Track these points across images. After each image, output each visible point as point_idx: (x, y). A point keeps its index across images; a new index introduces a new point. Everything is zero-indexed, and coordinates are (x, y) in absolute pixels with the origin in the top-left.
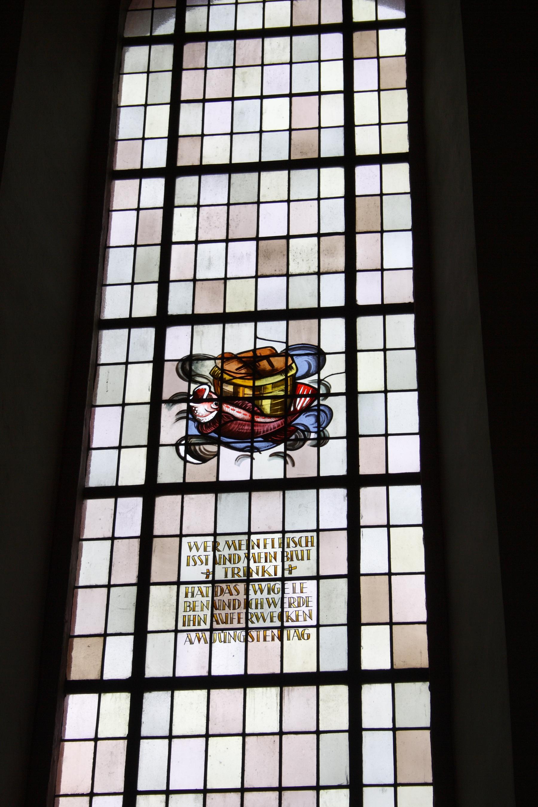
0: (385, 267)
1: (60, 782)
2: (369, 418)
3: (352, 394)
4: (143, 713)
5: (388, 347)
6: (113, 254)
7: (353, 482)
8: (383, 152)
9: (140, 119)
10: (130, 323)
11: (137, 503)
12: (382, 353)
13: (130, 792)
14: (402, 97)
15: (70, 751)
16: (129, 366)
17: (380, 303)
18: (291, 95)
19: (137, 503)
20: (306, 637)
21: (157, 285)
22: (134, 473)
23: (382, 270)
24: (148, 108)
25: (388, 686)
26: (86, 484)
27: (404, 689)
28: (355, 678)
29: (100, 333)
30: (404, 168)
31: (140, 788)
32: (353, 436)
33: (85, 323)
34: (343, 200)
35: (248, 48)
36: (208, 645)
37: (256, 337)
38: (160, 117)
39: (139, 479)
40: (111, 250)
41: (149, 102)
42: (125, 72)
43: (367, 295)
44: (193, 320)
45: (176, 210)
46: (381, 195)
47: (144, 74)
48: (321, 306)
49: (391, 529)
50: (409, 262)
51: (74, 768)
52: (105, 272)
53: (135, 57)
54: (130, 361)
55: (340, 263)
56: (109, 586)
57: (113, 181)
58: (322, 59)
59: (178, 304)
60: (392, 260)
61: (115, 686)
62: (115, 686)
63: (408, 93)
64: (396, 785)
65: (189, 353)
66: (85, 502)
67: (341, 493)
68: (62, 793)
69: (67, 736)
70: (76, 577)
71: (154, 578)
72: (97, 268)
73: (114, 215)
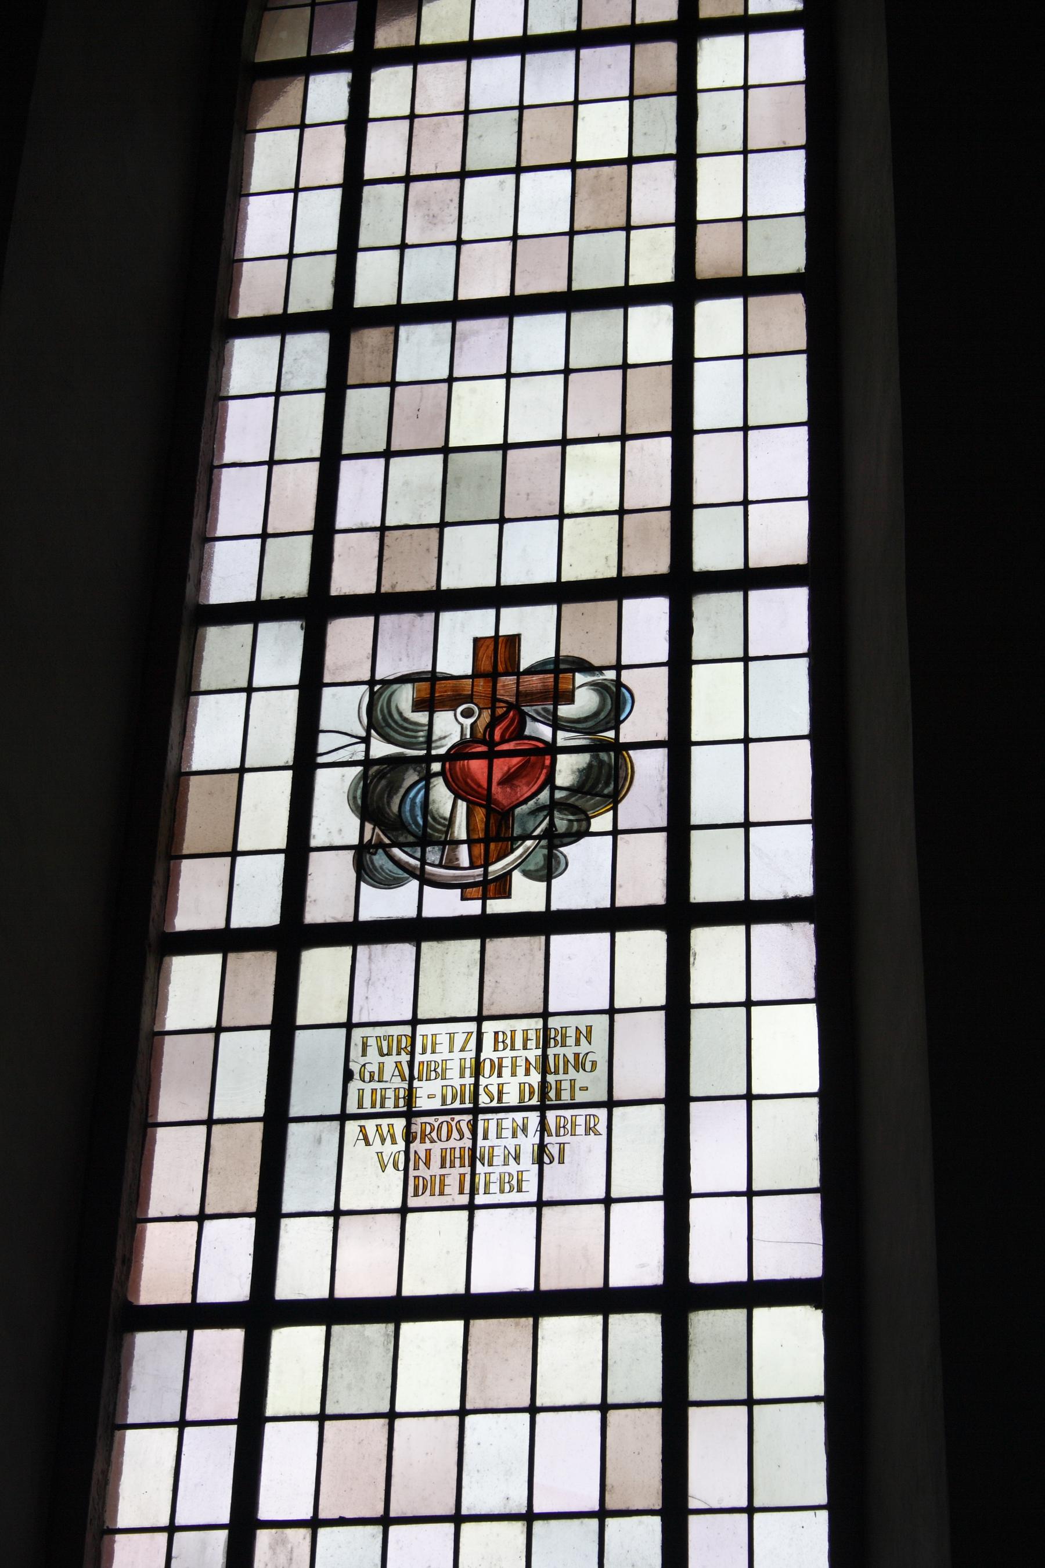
0: (757, 1517)
2: (713, 790)
3: (679, 744)
4: (309, 878)
5: (757, 1503)
6: (228, 479)
7: (678, 916)
8: (756, 1277)
9: (281, 223)
12: (743, 1010)
13: (244, 1523)
14: (798, 760)
18: (529, 1517)
19: (234, 1338)
20: (588, 1067)
21: (297, 692)
29: (228, 346)
32: (679, 829)
34: (664, 671)
35: (483, 337)
36: (401, 1174)
38: (322, 214)
40: (232, 404)
43: (712, 880)
44: (377, 604)
45: (327, 692)
47: (282, 261)
49: (742, 361)
56: (182, 1424)
57: (230, 341)
59: (352, 575)
60: (763, 492)
63: (821, 1103)
66: (201, 631)
67: (665, 313)
72: (177, 653)
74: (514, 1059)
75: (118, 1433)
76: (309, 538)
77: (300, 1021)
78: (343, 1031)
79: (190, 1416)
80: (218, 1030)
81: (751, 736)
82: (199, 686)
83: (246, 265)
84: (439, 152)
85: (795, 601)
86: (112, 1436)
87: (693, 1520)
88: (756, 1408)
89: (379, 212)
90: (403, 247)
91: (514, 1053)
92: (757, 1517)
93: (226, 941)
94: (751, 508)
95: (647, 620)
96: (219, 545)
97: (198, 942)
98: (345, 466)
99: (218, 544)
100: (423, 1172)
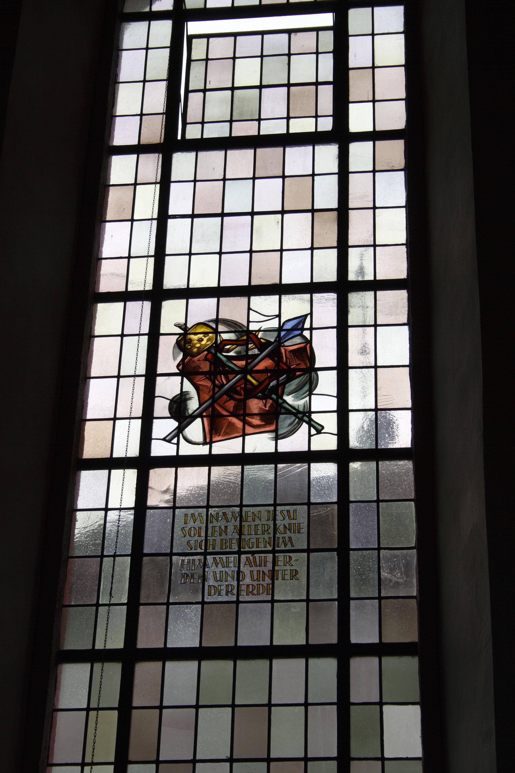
1: (91, 362)
3: (342, 368)
6: (61, 718)
10: (125, 296)
11: (132, 474)
14: (400, 217)
15: (62, 720)
16: (146, 84)
17: (373, 279)
19: (132, 474)
22: (127, 445)
23: (375, 246)
24: (132, 260)
25: (371, 143)
26: (87, 374)
27: (390, 662)
28: (344, 651)
30: (399, 145)
31: (171, 212)
33: (81, 294)
37: (249, 309)
39: (134, 451)
40: (124, 52)
41: (147, 79)
42: (107, 219)
44: (188, 293)
46: (373, 67)
48: (318, 130)
50: (402, 237)
51: (66, 734)
52: (113, 122)
53: (133, 34)
54: (118, 416)
55: (333, 239)
58: (320, 51)
61: (124, 463)
62: (124, 463)
64: (374, 171)
65: (179, 392)
68: (111, 184)
69: (88, 417)
70: (49, 750)
71: (132, 757)
73: (124, 54)
74: (257, 539)
75: (88, 380)
76: (164, 83)
77: (173, 179)
78: (109, 507)
79: (118, 416)
80: (135, 184)
81: (378, 365)
82: (86, 417)
83: (117, 119)
84: (209, 197)
85: (401, 296)
86: (86, 381)
87: (350, 330)
88: (377, 243)
89: (177, 233)
90: (190, 254)
91: (257, 536)
92: (378, 328)
93: (93, 656)
94: (376, 70)
95: (326, 307)
96: (92, 380)
97: (111, 297)
98: (170, 222)
99: (117, 118)
100: (215, 523)
